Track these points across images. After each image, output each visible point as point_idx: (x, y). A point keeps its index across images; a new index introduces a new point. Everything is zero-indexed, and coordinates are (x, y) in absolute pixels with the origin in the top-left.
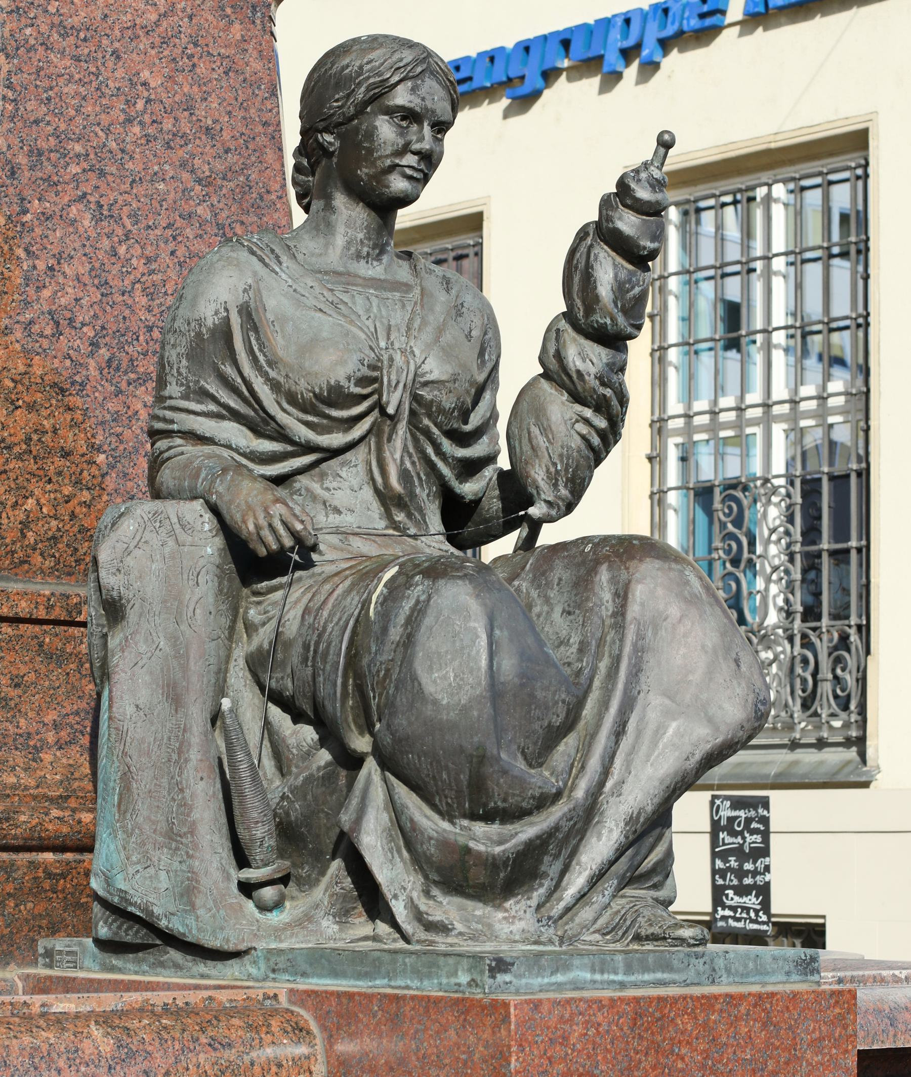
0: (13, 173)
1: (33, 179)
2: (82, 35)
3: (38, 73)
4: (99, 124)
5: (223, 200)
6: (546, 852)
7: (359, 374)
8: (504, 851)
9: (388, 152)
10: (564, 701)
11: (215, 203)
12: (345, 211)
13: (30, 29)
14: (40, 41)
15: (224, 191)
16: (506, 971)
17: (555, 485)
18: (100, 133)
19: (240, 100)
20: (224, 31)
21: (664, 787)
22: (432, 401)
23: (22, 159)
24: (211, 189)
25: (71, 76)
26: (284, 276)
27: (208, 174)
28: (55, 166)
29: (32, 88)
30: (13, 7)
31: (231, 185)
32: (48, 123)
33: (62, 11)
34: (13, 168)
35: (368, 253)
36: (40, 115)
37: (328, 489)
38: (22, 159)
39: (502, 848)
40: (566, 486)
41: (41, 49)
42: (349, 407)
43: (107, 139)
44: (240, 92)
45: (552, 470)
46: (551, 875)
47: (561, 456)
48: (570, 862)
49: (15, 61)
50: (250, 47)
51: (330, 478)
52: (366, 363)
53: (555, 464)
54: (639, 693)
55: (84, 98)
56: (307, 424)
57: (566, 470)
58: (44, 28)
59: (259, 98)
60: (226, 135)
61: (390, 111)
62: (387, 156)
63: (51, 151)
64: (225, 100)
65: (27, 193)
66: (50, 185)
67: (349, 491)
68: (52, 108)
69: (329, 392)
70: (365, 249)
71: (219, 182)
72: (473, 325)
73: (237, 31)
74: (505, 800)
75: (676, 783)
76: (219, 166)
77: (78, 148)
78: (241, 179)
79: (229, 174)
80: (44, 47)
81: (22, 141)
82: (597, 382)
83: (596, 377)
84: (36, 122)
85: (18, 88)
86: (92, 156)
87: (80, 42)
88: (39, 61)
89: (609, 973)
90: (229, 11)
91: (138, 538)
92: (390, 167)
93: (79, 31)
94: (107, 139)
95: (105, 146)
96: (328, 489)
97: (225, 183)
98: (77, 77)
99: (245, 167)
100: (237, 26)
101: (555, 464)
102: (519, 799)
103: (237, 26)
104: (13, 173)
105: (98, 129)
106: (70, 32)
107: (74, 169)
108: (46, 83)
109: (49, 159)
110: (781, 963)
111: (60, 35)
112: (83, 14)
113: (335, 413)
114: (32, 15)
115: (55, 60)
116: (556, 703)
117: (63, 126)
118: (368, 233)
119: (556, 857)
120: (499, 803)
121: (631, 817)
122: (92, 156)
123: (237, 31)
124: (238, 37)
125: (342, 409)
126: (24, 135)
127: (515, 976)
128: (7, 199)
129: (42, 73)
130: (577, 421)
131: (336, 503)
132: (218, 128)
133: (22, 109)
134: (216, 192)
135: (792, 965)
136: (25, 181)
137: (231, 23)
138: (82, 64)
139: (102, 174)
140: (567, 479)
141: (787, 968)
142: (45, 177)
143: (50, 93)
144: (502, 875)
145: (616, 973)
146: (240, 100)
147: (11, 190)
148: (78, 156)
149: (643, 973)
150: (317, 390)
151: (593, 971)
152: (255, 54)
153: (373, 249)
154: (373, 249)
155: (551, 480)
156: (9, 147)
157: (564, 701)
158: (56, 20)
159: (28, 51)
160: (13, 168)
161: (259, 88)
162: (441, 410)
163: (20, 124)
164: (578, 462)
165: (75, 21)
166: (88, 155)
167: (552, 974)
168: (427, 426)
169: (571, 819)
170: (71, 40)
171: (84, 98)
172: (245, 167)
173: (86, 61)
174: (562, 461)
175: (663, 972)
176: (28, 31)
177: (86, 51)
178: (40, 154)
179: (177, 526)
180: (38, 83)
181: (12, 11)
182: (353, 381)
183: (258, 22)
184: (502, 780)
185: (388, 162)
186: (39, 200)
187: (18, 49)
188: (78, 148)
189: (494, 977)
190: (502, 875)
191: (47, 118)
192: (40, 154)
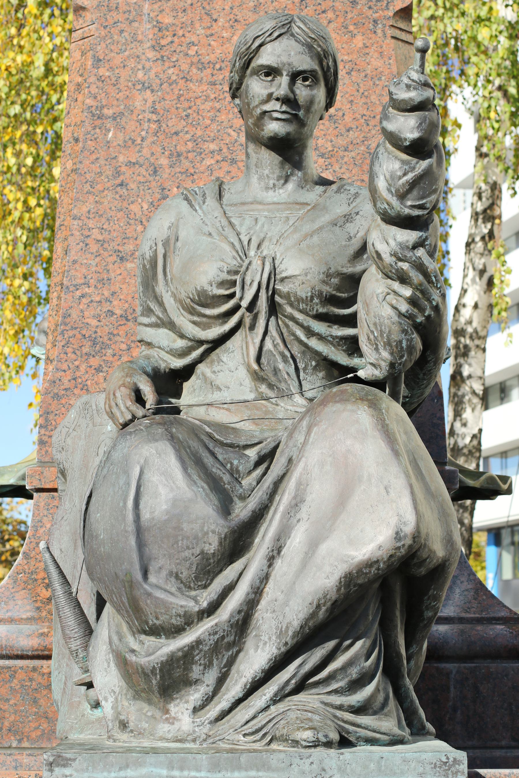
0: (155, 172)
1: (173, 174)
2: (218, 66)
3: (178, 98)
4: (231, 127)
5: (345, 167)
6: (193, 662)
7: (220, 280)
8: (149, 662)
9: (257, 103)
10: (213, 532)
11: (337, 169)
12: (254, 155)
13: (172, 69)
14: (182, 75)
15: (346, 159)
16: (64, 766)
17: (377, 349)
18: (233, 133)
19: (361, 91)
20: (347, 43)
21: (307, 603)
22: (288, 293)
23: (164, 161)
24: (333, 160)
25: (207, 97)
26: (200, 211)
27: (330, 149)
28: (192, 162)
29: (173, 110)
30: (159, 56)
31: (353, 154)
32: (187, 133)
33: (200, 52)
34: (155, 168)
35: (274, 185)
36: (179, 128)
37: (214, 372)
38: (164, 161)
39: (147, 659)
40: (385, 349)
41: (182, 82)
42: (219, 306)
43: (238, 136)
44: (361, 85)
45: (372, 337)
46: (207, 682)
47: (375, 324)
48: (229, 670)
49: (159, 93)
50: (372, 51)
51: (216, 363)
52: (225, 269)
53: (372, 332)
54: (299, 521)
55: (219, 111)
56: (194, 323)
57: (382, 335)
58: (185, 67)
59: (380, 87)
60: (348, 118)
61: (256, 72)
62: (257, 106)
63: (189, 152)
64: (347, 92)
65: (167, 185)
66: (187, 176)
67: (227, 372)
68: (190, 121)
69: (199, 296)
70: (271, 182)
71: (341, 153)
72: (361, 227)
73: (359, 41)
74: (157, 618)
75: (319, 600)
76: (341, 142)
77: (213, 146)
78: (362, 148)
79: (350, 147)
80: (184, 80)
81: (164, 149)
82: (394, 259)
83: (391, 255)
84: (177, 133)
85: (162, 112)
86: (225, 150)
87: (215, 72)
88: (180, 90)
89: (189, 770)
90: (351, 28)
91: (75, 423)
92: (261, 114)
93: (214, 64)
94: (238, 136)
95: (236, 141)
96: (214, 372)
97: (346, 153)
98: (212, 96)
99: (366, 138)
100: (359, 37)
101: (372, 332)
102: (167, 617)
103: (359, 37)
104: (155, 172)
105: (230, 131)
106: (207, 66)
107: (209, 162)
108: (186, 105)
109: (187, 158)
110: (413, 765)
111: (199, 69)
112: (219, 52)
113: (208, 312)
114: (174, 59)
115: (194, 87)
116: (207, 533)
117: (199, 133)
118: (272, 169)
119: (208, 666)
120: (155, 621)
121: (281, 631)
122: (225, 150)
123: (359, 41)
124: (360, 45)
125: (213, 307)
126: (166, 144)
127: (77, 771)
128: (150, 191)
129: (182, 99)
130: (388, 294)
131: (218, 382)
132: (340, 114)
133: (164, 126)
134: (337, 161)
135: (428, 768)
136: (165, 176)
137: (353, 36)
138: (217, 86)
139: (233, 161)
140: (384, 342)
141: (421, 770)
142: (183, 171)
143: (189, 111)
144: (154, 682)
145: (198, 770)
146: (361, 91)
147: (154, 184)
148: (212, 152)
149: (233, 771)
150: (191, 296)
151: (171, 767)
152: (376, 55)
153: (278, 180)
154: (278, 180)
155: (372, 345)
156: (153, 154)
157: (213, 532)
158: (195, 60)
159: (170, 85)
160: (155, 168)
161: (380, 79)
162: (299, 300)
163: (162, 137)
164: (390, 328)
165: (212, 58)
166: (221, 150)
167: (121, 769)
168: (291, 314)
169: (216, 633)
170: (209, 71)
171: (219, 111)
172: (366, 138)
173: (221, 84)
174: (376, 328)
175: (258, 770)
176: (171, 71)
177: (221, 77)
178: (179, 155)
179: (95, 412)
180: (178, 105)
181: (157, 59)
182: (214, 286)
183: (379, 31)
184: (148, 601)
185: (259, 111)
186: (178, 187)
187: (161, 85)
188: (213, 146)
189: (51, 771)
190: (154, 682)
191: (186, 129)
192: (179, 155)
